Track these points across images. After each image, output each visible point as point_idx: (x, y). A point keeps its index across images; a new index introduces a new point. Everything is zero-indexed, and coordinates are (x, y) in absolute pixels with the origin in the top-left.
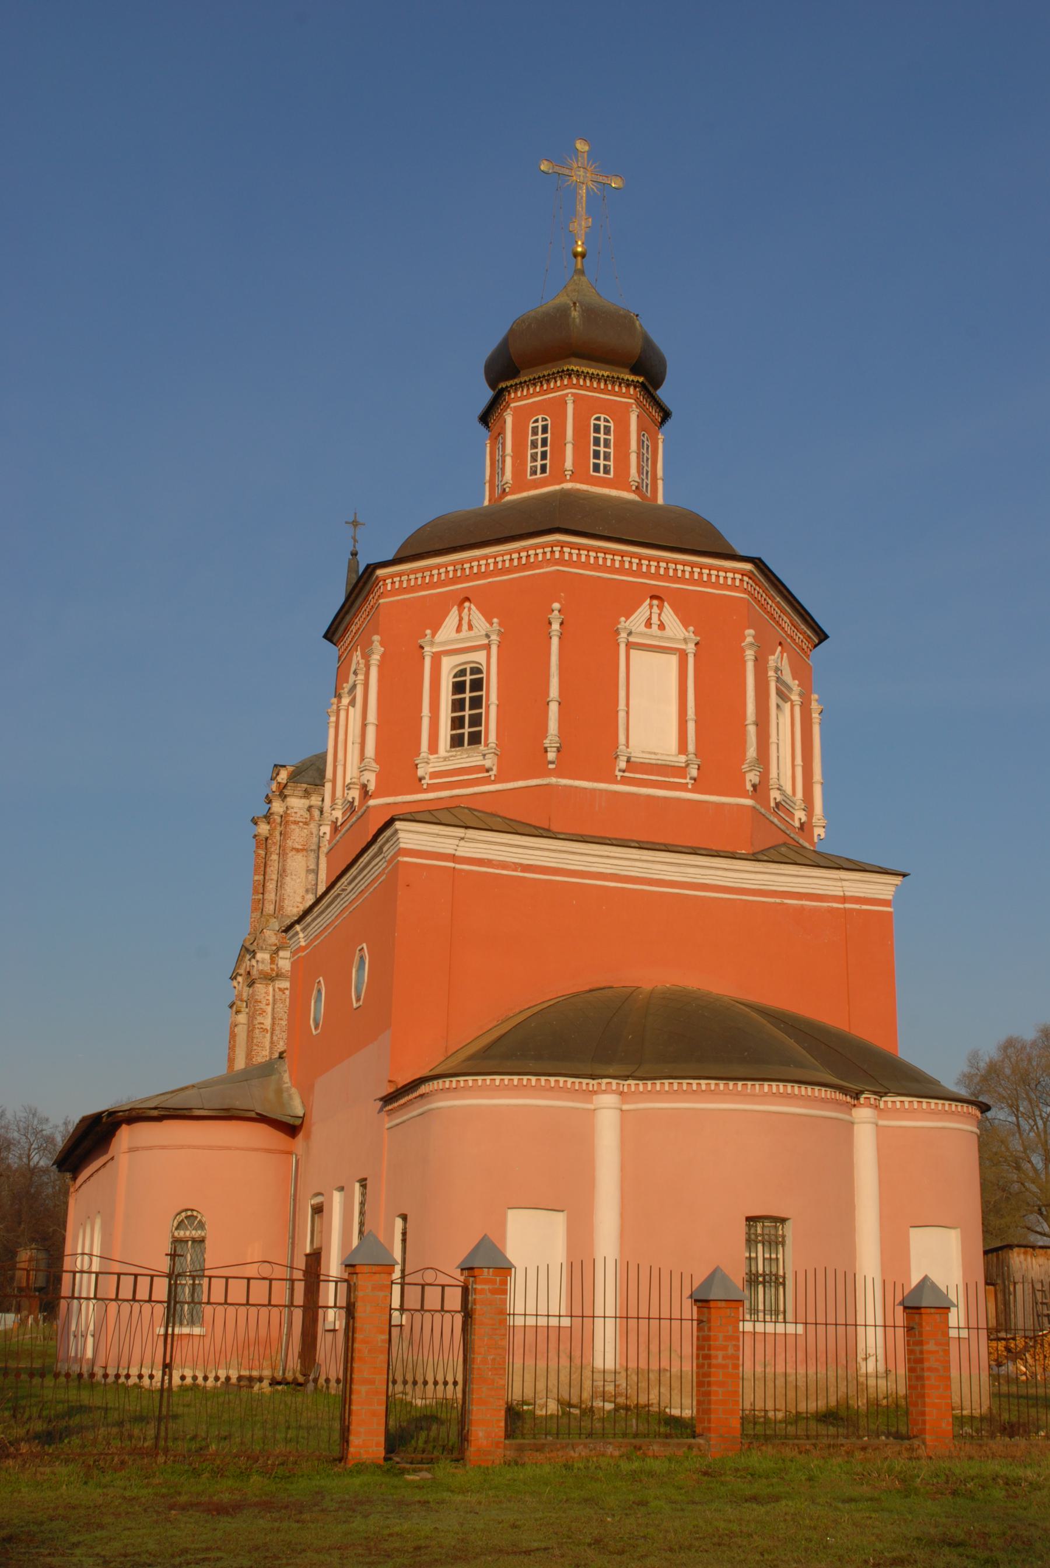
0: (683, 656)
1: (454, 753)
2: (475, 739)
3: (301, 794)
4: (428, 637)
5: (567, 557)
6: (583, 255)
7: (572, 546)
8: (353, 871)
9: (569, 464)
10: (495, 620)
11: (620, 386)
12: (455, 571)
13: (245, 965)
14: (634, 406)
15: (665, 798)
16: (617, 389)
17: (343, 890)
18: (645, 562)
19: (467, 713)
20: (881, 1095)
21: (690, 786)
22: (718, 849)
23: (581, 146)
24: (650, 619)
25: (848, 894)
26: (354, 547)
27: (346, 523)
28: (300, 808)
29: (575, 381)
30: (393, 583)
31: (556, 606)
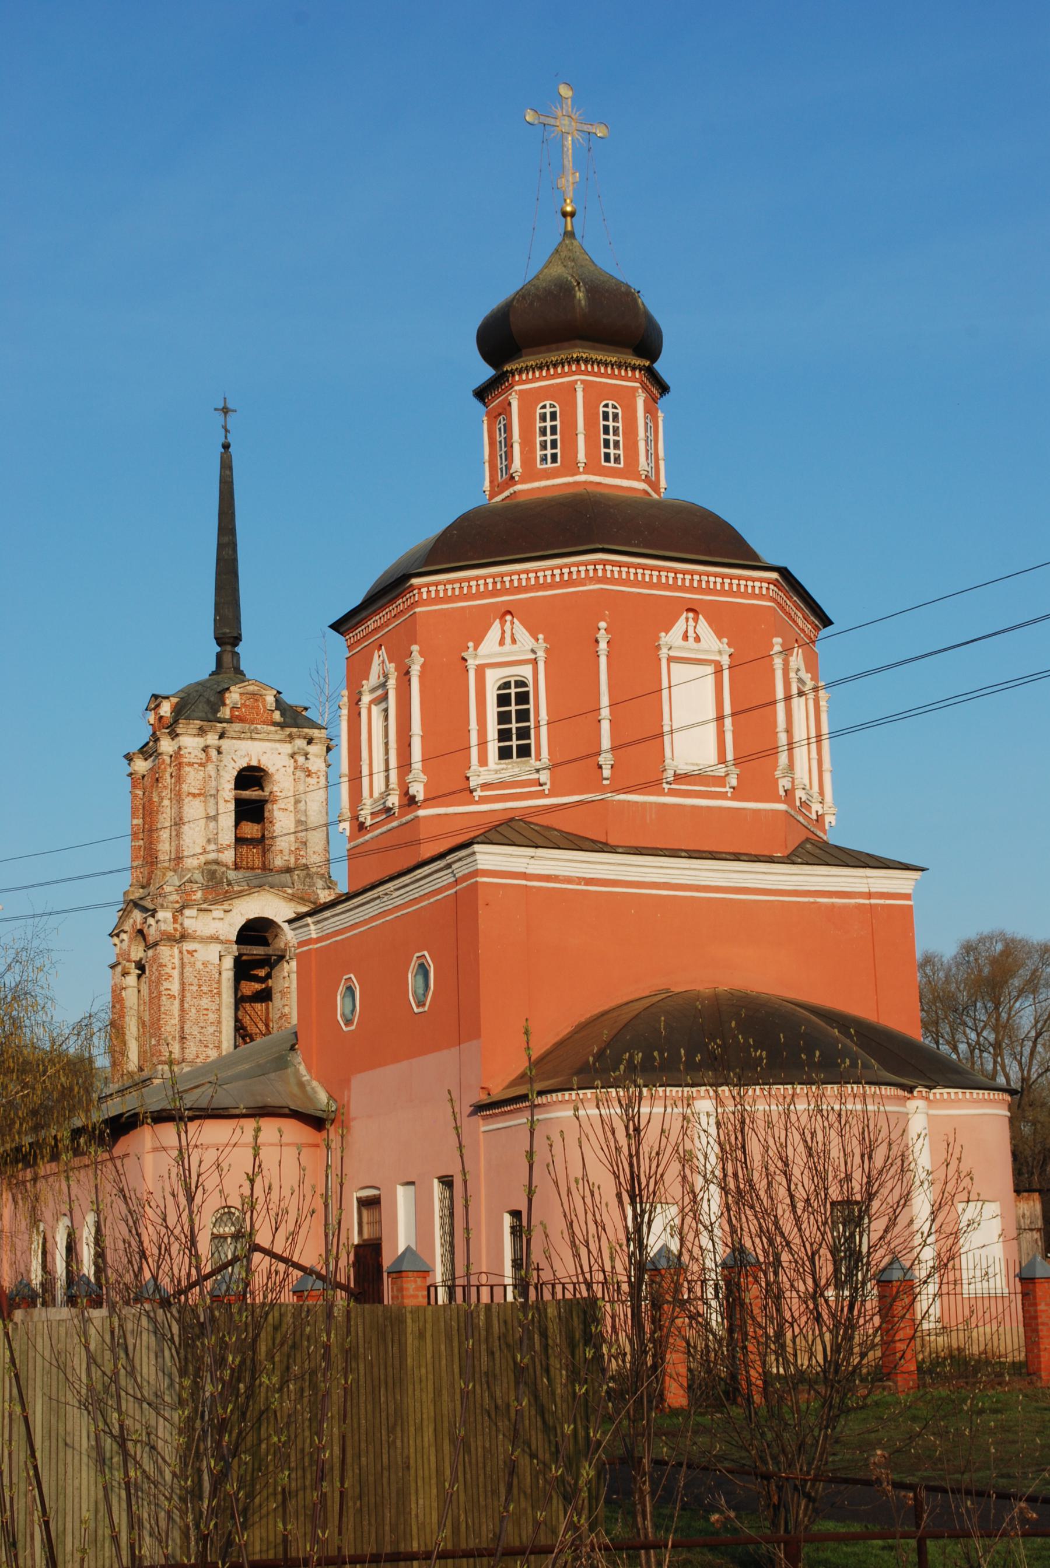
0: (718, 671)
1: (504, 766)
2: (524, 752)
3: (195, 732)
4: (471, 649)
5: (609, 575)
6: (572, 215)
7: (614, 564)
8: (406, 879)
9: (581, 456)
10: (541, 636)
11: (626, 370)
12: (495, 583)
13: (131, 921)
14: (640, 391)
15: (708, 808)
16: (623, 373)
17: (386, 894)
18: (680, 576)
19: (514, 726)
20: (930, 1088)
21: (729, 795)
22: (757, 853)
23: (565, 91)
24: (687, 631)
25: (873, 890)
26: (226, 437)
27: (216, 409)
28: (194, 748)
29: (583, 367)
30: (429, 592)
31: (603, 625)
